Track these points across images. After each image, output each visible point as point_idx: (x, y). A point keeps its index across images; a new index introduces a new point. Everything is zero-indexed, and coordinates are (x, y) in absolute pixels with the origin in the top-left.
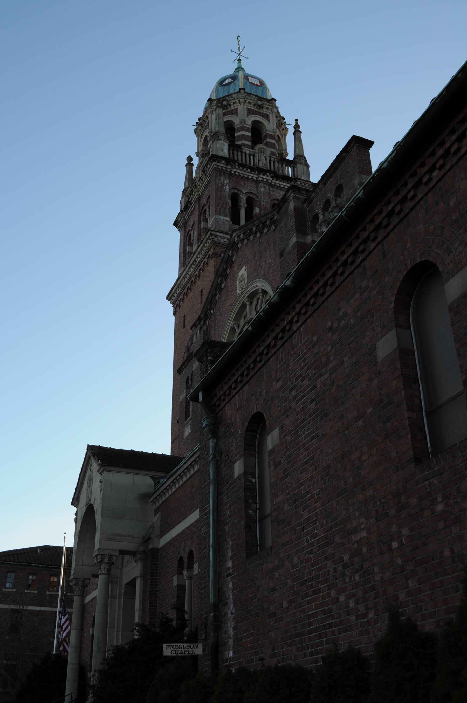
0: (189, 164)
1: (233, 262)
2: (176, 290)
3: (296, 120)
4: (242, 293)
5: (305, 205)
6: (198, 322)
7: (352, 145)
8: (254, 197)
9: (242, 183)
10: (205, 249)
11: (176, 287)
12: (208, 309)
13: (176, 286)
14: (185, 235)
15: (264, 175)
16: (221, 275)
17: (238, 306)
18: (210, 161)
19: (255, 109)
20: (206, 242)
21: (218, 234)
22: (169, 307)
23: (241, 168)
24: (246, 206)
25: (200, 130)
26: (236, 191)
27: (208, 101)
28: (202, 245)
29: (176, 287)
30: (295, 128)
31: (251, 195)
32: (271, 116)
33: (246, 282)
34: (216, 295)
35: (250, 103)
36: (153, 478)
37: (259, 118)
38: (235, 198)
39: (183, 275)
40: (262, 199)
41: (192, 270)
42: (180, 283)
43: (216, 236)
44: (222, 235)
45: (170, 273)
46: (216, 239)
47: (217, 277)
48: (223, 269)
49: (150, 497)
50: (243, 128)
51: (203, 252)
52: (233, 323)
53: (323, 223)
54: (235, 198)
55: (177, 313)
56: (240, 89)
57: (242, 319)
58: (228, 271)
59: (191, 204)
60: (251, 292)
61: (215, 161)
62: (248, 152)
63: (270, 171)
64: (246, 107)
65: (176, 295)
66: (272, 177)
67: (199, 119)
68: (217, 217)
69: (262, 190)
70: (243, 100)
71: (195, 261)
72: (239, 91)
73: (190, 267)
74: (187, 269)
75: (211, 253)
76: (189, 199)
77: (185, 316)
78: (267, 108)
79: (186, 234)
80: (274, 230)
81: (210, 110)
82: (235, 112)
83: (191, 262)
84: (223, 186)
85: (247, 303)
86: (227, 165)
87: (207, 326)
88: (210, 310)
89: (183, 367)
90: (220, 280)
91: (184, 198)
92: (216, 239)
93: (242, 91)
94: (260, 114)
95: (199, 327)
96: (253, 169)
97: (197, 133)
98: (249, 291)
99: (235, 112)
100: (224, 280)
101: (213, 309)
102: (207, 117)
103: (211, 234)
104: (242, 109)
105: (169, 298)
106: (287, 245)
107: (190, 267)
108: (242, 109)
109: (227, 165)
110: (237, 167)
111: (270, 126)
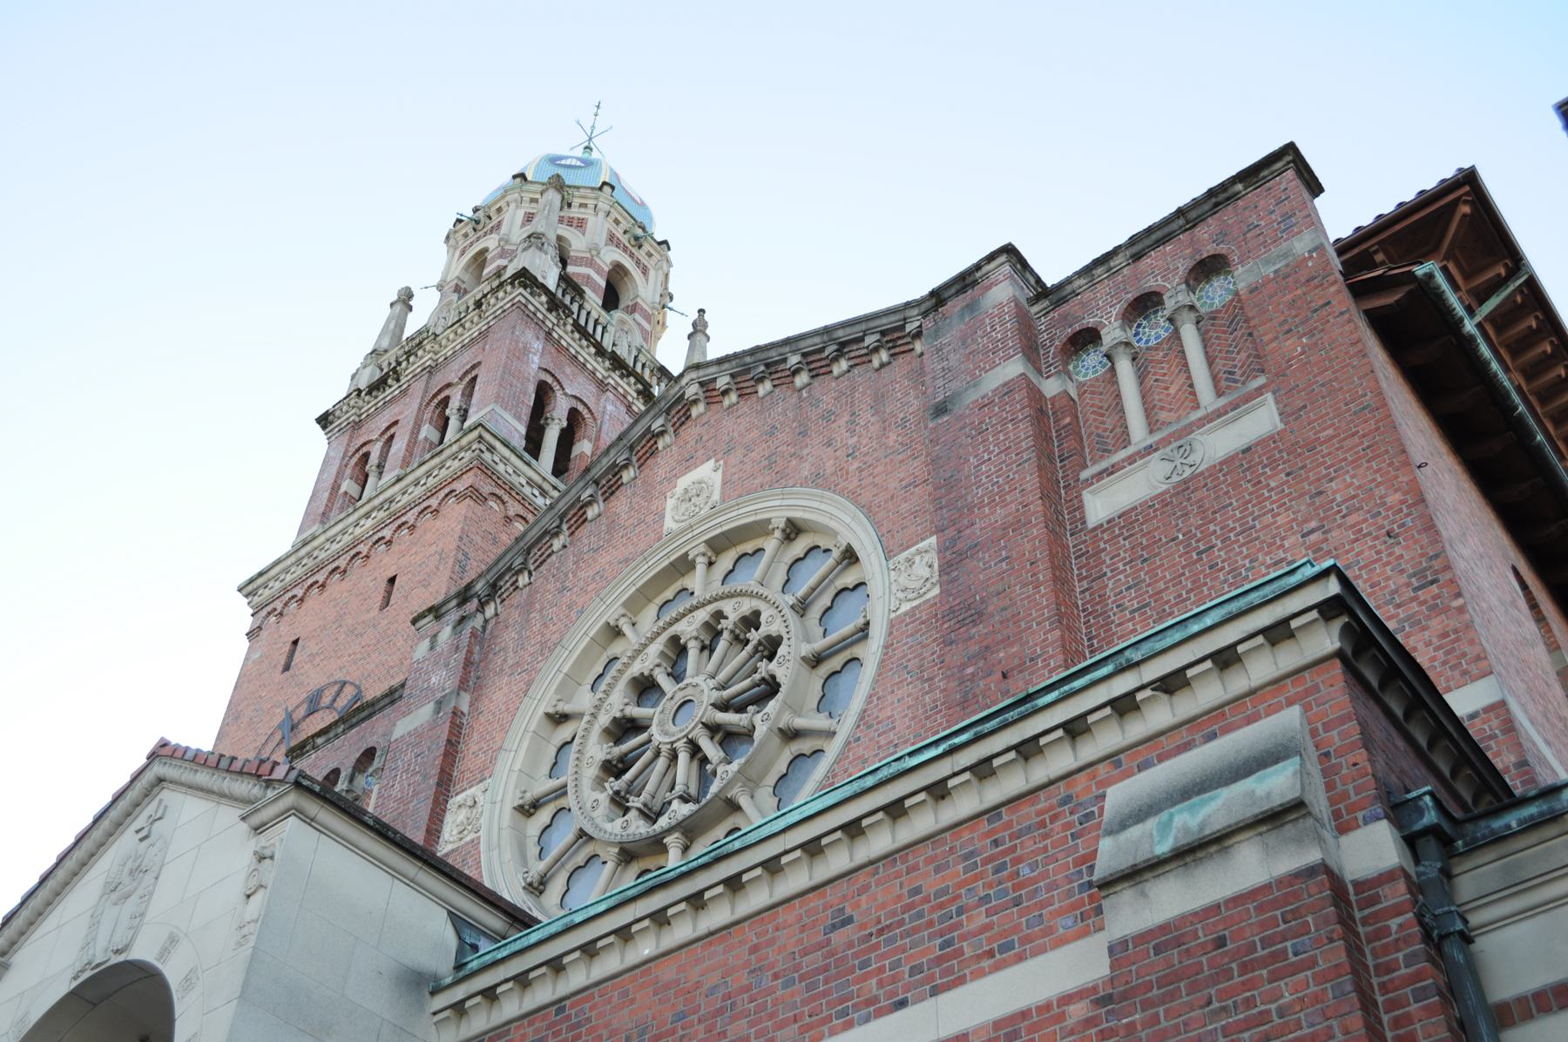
0: (405, 300)
1: (653, 452)
2: (286, 571)
3: (701, 311)
4: (683, 532)
5: (1035, 309)
6: (454, 603)
7: (1279, 165)
8: (585, 412)
9: (568, 370)
10: (444, 472)
11: (289, 562)
12: (509, 569)
13: (293, 559)
14: (346, 451)
15: (622, 376)
16: (597, 483)
17: (659, 561)
18: (512, 284)
19: (624, 239)
20: (454, 457)
21: (498, 445)
22: (241, 615)
23: (577, 335)
24: (565, 424)
25: (466, 235)
26: (549, 380)
27: (514, 177)
28: (437, 460)
29: (289, 562)
30: (694, 325)
31: (580, 408)
32: (652, 273)
33: (716, 496)
34: (556, 535)
35: (617, 222)
36: (458, 920)
37: (628, 263)
38: (543, 394)
39: (254, 585)
40: (605, 427)
41: (369, 523)
42: (309, 555)
43: (491, 449)
44: (506, 452)
45: (272, 527)
46: (487, 456)
47: (581, 484)
48: (614, 465)
49: (434, 993)
50: (590, 263)
51: (431, 481)
52: (622, 611)
53: (1121, 349)
54: (543, 394)
55: (264, 634)
56: (604, 183)
57: (652, 610)
58: (627, 476)
59: (398, 380)
60: (725, 528)
61: (525, 287)
62: (594, 315)
63: (640, 379)
64: (607, 226)
65: (278, 585)
66: (639, 393)
67: (476, 210)
68: (499, 410)
69: (610, 408)
70: (607, 208)
71: (391, 501)
72: (601, 189)
73: (367, 515)
74: (351, 519)
75: (459, 486)
76: (399, 364)
77: (295, 642)
78: (650, 255)
79: (352, 450)
80: (882, 365)
81: (516, 196)
82: (580, 224)
83: (376, 502)
84: (526, 350)
85: (700, 560)
86: (549, 310)
87: (486, 621)
88: (520, 571)
89: (319, 741)
90: (589, 492)
91: (368, 370)
92: (487, 456)
93: (607, 189)
94: (632, 255)
95: (453, 616)
96: (600, 352)
97: (452, 241)
98: (720, 524)
99: (580, 224)
100: (600, 499)
101: (530, 574)
102: (499, 210)
103: (480, 436)
104: (598, 227)
105: (250, 588)
106: (975, 382)
107: (367, 515)
108: (598, 227)
109: (549, 310)
110: (569, 328)
111: (643, 289)
